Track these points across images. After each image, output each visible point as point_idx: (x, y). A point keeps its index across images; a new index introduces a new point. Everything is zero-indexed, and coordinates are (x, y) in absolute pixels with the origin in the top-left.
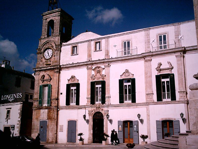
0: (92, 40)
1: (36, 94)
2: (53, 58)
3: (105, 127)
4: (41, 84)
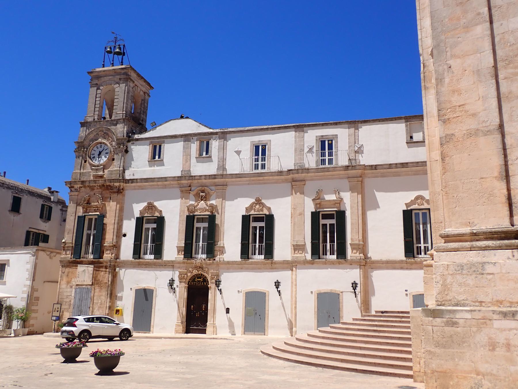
1: (68, 233)
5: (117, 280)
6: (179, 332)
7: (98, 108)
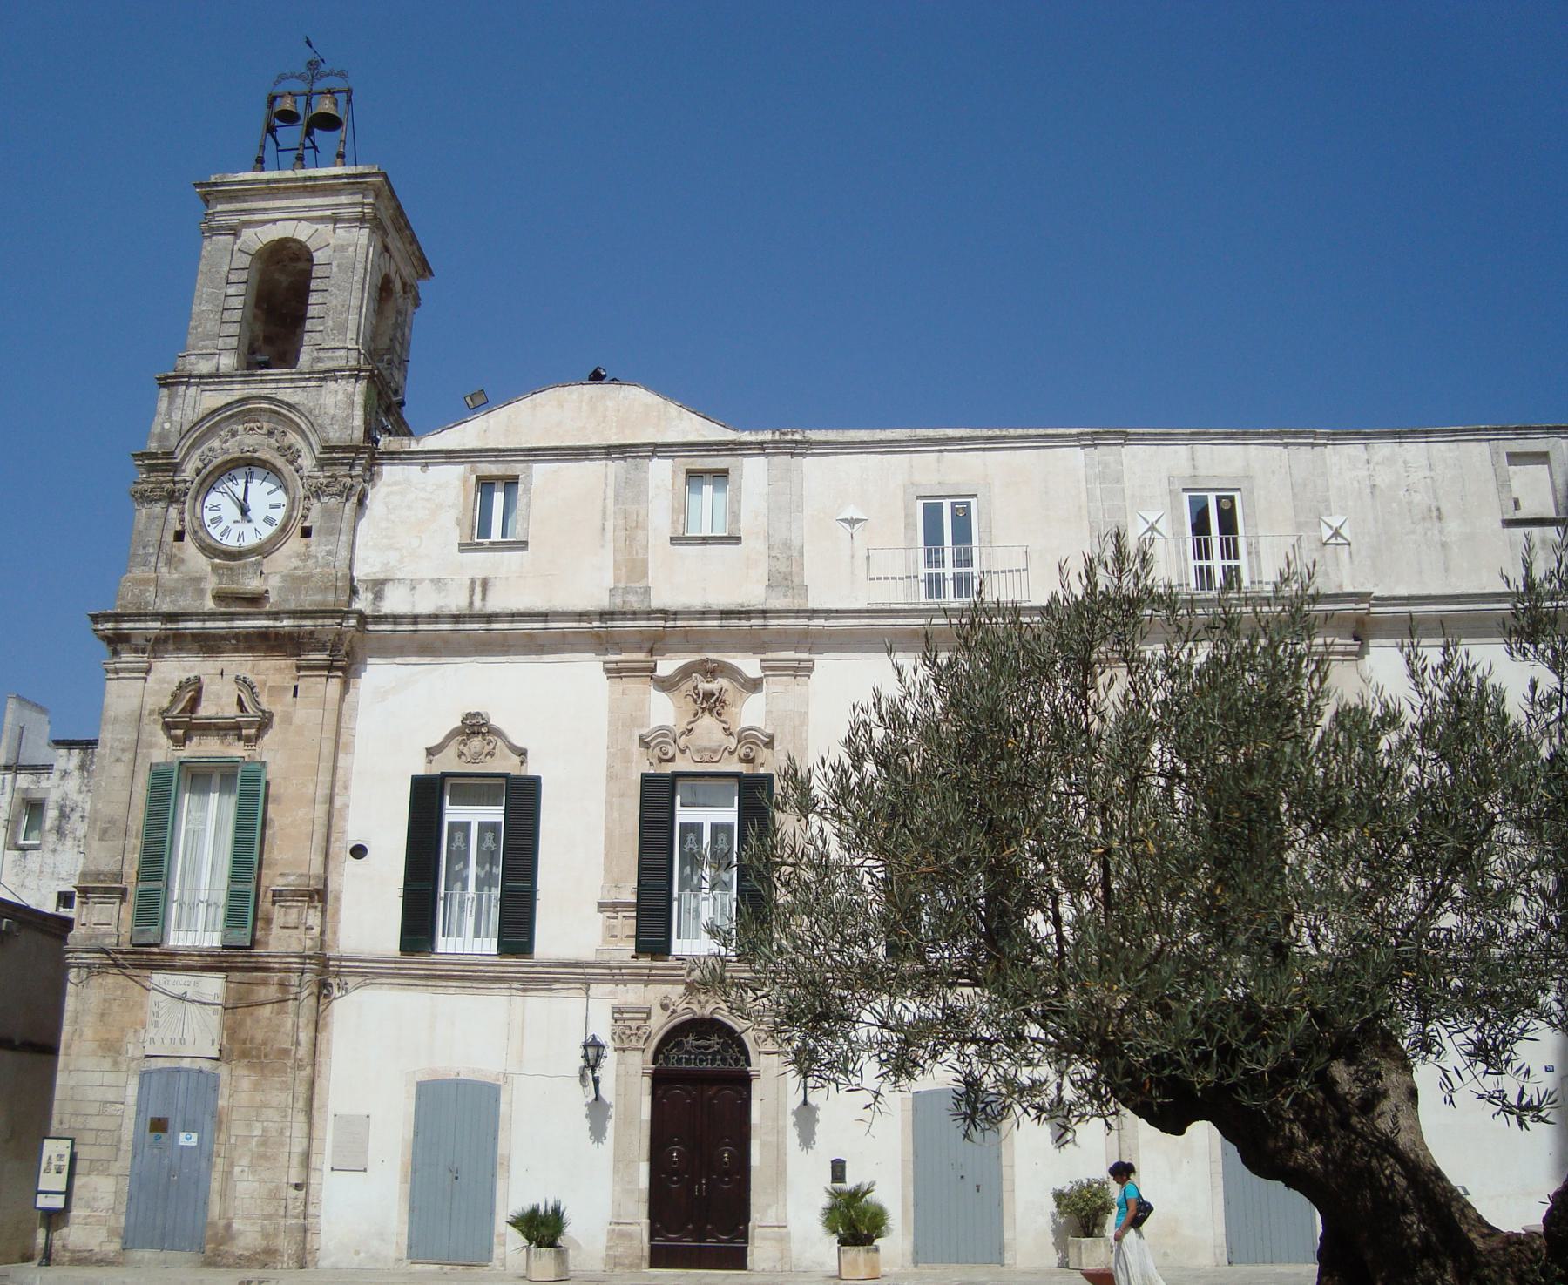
0: (658, 449)
2: (295, 543)
3: (762, 1146)
4: (162, 751)
5: (329, 1042)
6: (627, 1262)
7: (237, 325)
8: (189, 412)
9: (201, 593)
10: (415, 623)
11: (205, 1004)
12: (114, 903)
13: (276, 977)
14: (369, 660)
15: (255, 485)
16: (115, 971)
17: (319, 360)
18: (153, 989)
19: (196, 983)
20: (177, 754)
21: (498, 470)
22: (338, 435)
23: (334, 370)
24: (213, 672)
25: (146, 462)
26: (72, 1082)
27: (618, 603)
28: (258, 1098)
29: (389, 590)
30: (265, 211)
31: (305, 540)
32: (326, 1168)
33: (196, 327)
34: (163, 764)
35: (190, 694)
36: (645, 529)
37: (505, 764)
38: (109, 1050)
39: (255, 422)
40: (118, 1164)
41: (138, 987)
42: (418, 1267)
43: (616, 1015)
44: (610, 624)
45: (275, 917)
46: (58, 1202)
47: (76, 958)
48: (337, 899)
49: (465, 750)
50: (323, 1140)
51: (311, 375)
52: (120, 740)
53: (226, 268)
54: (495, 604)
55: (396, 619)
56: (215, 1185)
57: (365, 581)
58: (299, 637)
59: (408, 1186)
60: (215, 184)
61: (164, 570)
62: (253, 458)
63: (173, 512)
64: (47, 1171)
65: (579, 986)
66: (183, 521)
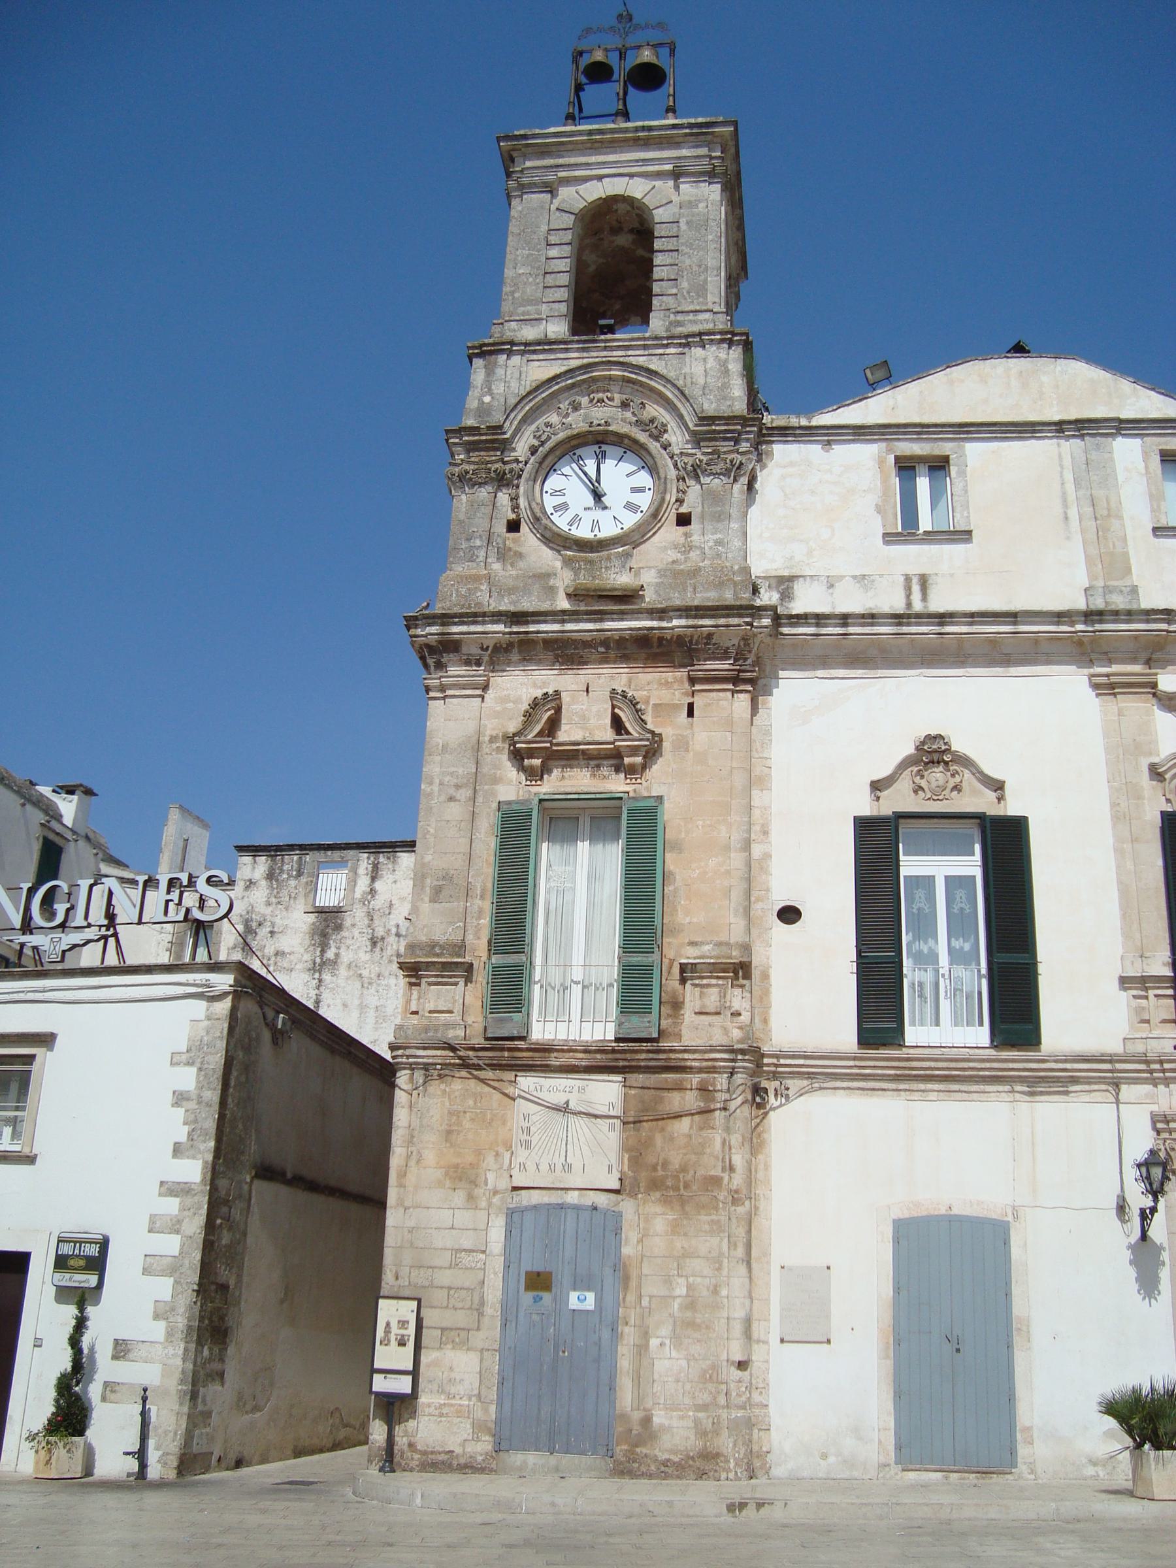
0: (1122, 426)
2: (669, 533)
5: (767, 1167)
8: (514, 385)
9: (551, 591)
10: (845, 625)
11: (596, 1116)
12: (456, 984)
13: (695, 1079)
14: (782, 674)
15: (608, 465)
16: (464, 1073)
17: (679, 324)
18: (520, 1096)
19: (581, 1090)
20: (534, 789)
21: (922, 449)
22: (714, 405)
23: (700, 334)
24: (574, 687)
25: (466, 438)
26: (412, 1224)
27: (1099, 603)
28: (678, 1245)
29: (799, 587)
30: (587, 165)
31: (682, 529)
32: (774, 1339)
33: (513, 292)
34: (517, 802)
35: (549, 713)
36: (1120, 518)
37: (982, 802)
38: (461, 1180)
39: (604, 391)
40: (481, 1335)
41: (497, 1096)
42: (912, 1475)
43: (1160, 1125)
44: (1098, 627)
45: (687, 1000)
46: (403, 1385)
47: (408, 1057)
48: (766, 976)
49: (923, 783)
50: (767, 1301)
51: (668, 340)
52: (452, 774)
53: (544, 228)
54: (938, 604)
55: (819, 619)
56: (625, 1363)
57: (765, 578)
58: (691, 642)
59: (890, 1363)
60: (525, 137)
61: (497, 566)
62: (607, 432)
63: (503, 498)
64: (386, 1342)
65: (1103, 1087)
66: (518, 506)
